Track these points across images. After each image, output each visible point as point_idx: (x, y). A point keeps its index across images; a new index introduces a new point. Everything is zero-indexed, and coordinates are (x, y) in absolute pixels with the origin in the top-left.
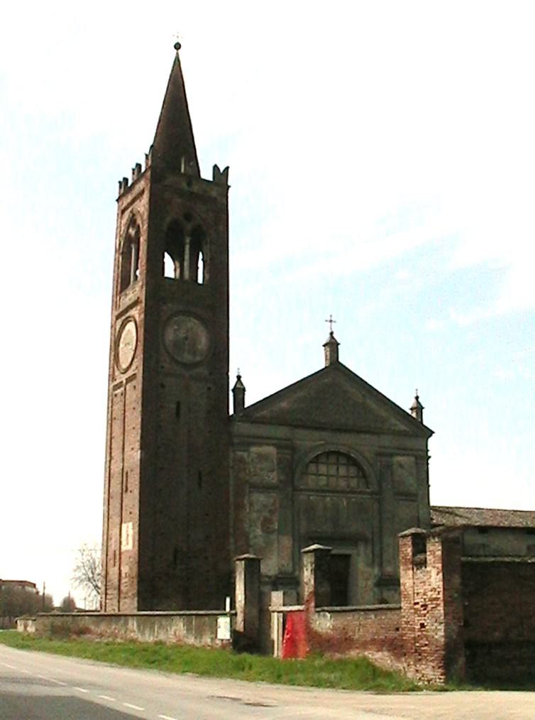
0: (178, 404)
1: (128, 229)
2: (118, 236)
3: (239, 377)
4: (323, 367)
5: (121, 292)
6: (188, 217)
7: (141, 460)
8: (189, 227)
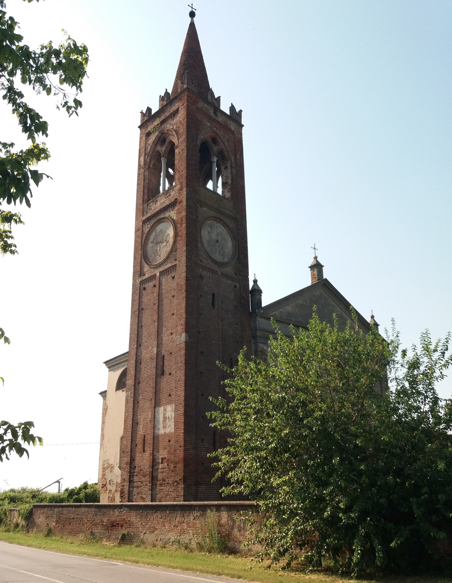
0: (213, 295)
1: (156, 146)
2: (143, 155)
3: (255, 281)
4: (311, 284)
5: (149, 200)
6: (214, 141)
7: (186, 342)
8: (216, 149)
